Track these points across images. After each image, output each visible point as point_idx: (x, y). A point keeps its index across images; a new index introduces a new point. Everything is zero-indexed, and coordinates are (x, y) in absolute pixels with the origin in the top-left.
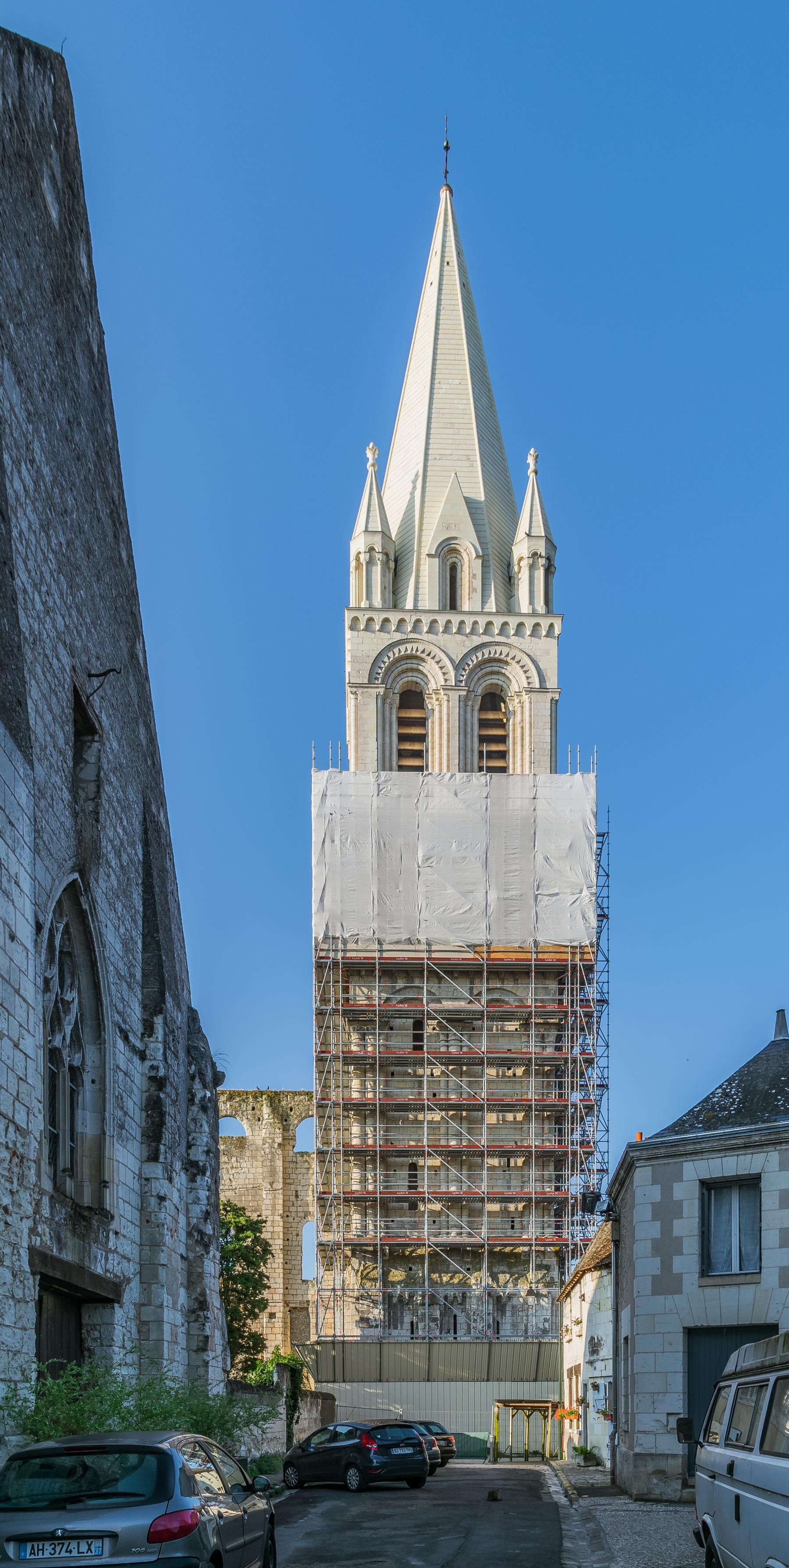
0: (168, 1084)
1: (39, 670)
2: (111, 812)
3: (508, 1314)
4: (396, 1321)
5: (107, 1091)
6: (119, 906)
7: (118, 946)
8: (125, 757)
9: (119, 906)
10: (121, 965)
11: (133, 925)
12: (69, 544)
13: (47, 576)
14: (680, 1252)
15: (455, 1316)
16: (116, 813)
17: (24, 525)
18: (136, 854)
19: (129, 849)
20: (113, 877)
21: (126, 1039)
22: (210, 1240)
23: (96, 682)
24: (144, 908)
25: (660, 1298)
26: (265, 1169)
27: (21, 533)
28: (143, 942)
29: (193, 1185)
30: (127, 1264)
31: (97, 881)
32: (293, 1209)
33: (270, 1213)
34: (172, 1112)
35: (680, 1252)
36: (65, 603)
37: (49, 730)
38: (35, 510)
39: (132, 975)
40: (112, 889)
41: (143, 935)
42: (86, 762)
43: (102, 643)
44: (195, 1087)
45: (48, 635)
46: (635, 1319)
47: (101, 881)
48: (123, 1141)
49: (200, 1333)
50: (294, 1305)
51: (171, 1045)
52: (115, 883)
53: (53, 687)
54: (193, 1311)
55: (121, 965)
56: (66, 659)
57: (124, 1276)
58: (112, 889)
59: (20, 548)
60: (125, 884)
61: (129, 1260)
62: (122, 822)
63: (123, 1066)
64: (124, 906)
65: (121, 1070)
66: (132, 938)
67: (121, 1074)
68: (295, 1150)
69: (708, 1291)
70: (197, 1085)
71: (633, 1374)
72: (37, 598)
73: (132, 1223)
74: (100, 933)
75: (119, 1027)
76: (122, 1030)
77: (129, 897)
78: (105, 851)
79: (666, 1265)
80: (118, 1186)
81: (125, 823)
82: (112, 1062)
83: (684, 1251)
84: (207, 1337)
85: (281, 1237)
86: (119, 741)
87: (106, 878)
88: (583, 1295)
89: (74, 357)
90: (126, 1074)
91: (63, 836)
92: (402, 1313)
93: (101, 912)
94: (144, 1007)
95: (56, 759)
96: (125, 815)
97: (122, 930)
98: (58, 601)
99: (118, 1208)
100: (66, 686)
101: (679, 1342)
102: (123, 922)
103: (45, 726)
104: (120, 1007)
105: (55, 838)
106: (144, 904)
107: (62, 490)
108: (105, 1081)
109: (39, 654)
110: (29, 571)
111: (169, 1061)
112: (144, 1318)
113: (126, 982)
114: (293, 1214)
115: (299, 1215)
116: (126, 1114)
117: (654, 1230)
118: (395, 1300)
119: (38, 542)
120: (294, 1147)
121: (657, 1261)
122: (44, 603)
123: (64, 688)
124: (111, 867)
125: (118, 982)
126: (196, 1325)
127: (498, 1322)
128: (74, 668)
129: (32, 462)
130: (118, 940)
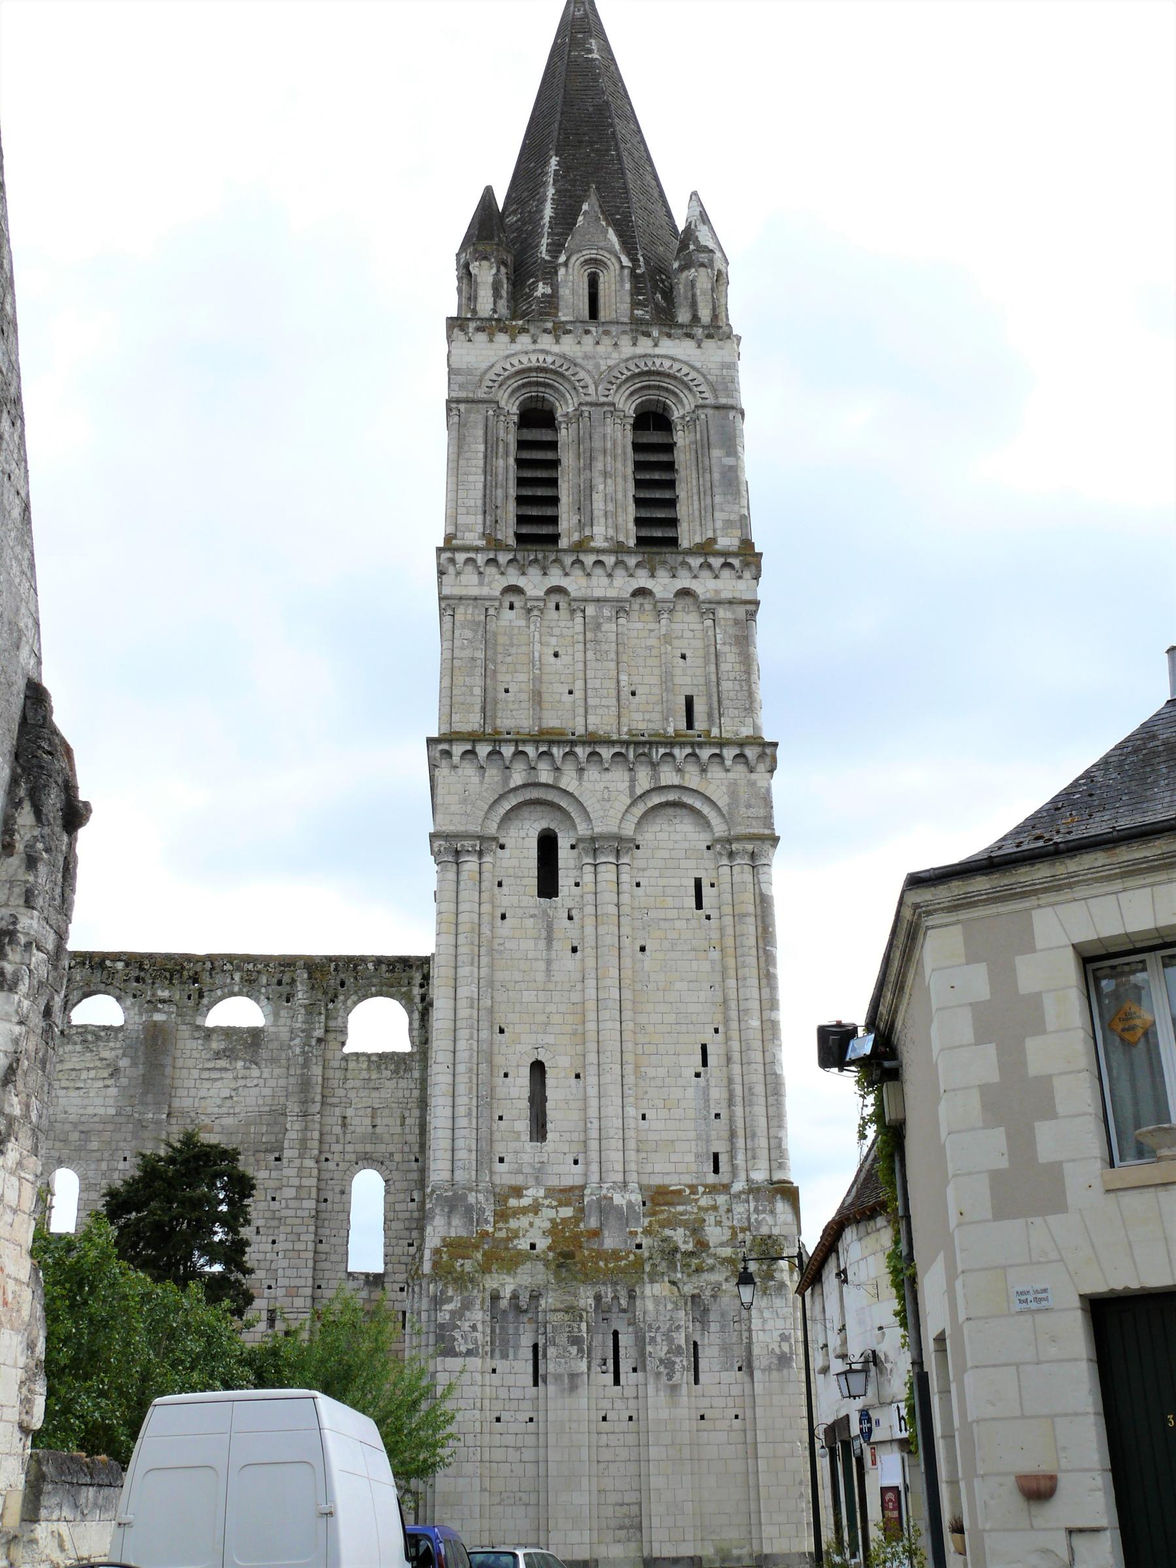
3: (714, 1327)
4: (505, 1343)
14: (1050, 1113)
15: (616, 1334)
25: (1013, 1227)
26: (292, 1080)
32: (337, 1148)
33: (295, 1153)
35: (1050, 1113)
44: (20, 821)
46: (958, 1284)
50: (331, 1318)
68: (347, 1050)
69: (1132, 1200)
71: (966, 1426)
79: (1021, 1144)
83: (1060, 1109)
85: (314, 1195)
88: (844, 1271)
92: (517, 1328)
101: (1073, 1337)
114: (337, 1157)
115: (347, 1157)
117: (984, 1064)
118: (504, 1304)
120: (343, 1044)
121: (998, 1136)
127: (695, 1344)
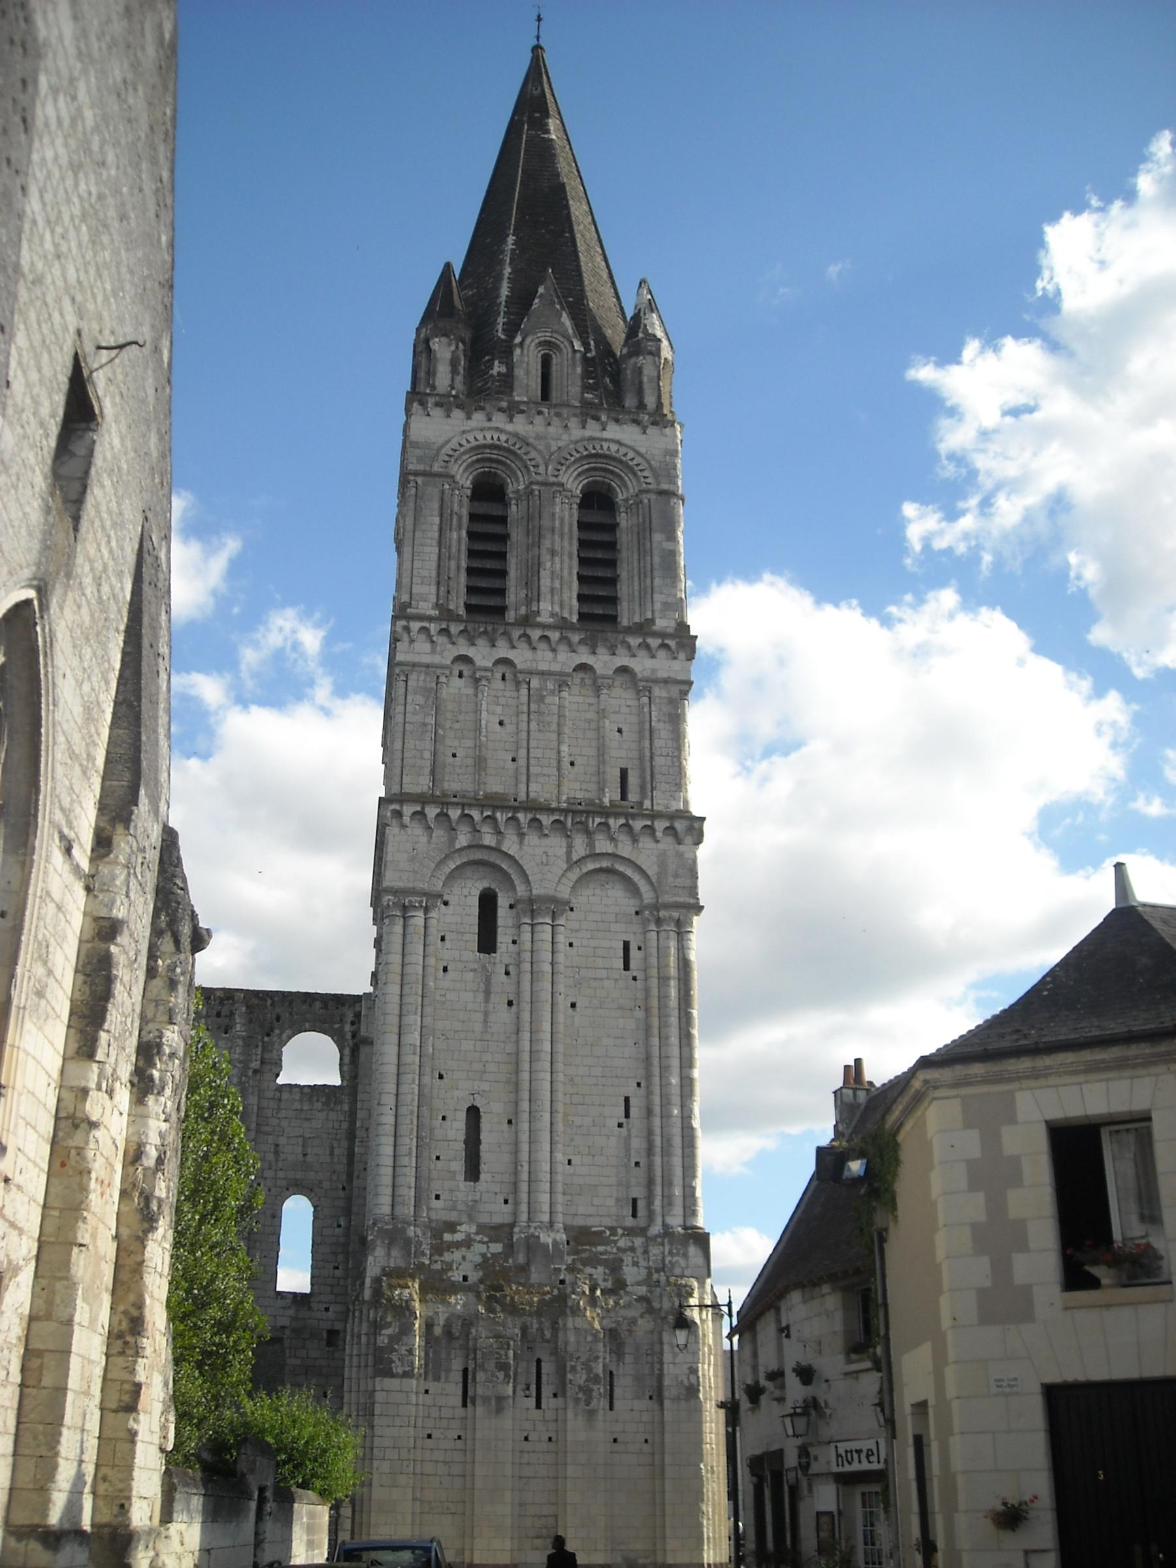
0: (126, 932)
1: (32, 316)
2: (97, 523)
5: (25, 931)
6: (87, 652)
7: (78, 710)
8: (127, 462)
9: (87, 652)
10: (76, 738)
11: (103, 684)
12: (101, 197)
13: (66, 218)
16: (103, 528)
17: (49, 154)
18: (122, 589)
19: (113, 579)
20: (85, 610)
21: (68, 851)
22: (159, 1207)
23: (105, 355)
24: (122, 665)
27: (43, 159)
28: (114, 714)
29: (140, 1109)
30: (16, 1238)
31: (61, 608)
34: (126, 978)
36: (83, 257)
37: (31, 392)
38: (66, 145)
39: (91, 758)
40: (80, 626)
41: (116, 703)
42: (72, 455)
43: (121, 320)
45: (54, 282)
47: (67, 611)
48: (38, 1018)
49: (127, 1376)
51: (138, 870)
52: (87, 619)
53: (48, 342)
54: (120, 1336)
55: (76, 738)
56: (72, 321)
57: (10, 1262)
58: (80, 626)
59: (38, 174)
60: (100, 625)
61: (21, 1231)
62: (109, 542)
63: (56, 894)
64: (94, 654)
65: (53, 900)
66: (98, 703)
67: (51, 908)
70: (166, 944)
72: (48, 236)
73: (36, 1164)
74: (54, 684)
75: (61, 833)
76: (62, 837)
77: (104, 645)
78: (79, 570)
80: (20, 1094)
81: (114, 544)
82: (41, 884)
84: (139, 1386)
86: (122, 439)
87: (75, 608)
89: (143, 29)
90: (59, 908)
91: (23, 532)
93: (59, 653)
94: (102, 807)
95: (33, 429)
96: (116, 534)
97: (86, 688)
98: (74, 250)
99: (15, 1134)
100: (65, 349)
102: (89, 677)
103: (28, 385)
104: (66, 802)
105: (11, 531)
106: (123, 660)
107: (103, 142)
108: (23, 914)
109: (37, 298)
110: (44, 204)
111: (132, 895)
112: (36, 1345)
113: (81, 765)
116: (50, 973)
119: (63, 179)
122: (56, 245)
123: (61, 348)
124: (83, 594)
125: (69, 761)
126: (120, 1361)
128: (79, 333)
129: (74, 98)
130: (78, 700)
